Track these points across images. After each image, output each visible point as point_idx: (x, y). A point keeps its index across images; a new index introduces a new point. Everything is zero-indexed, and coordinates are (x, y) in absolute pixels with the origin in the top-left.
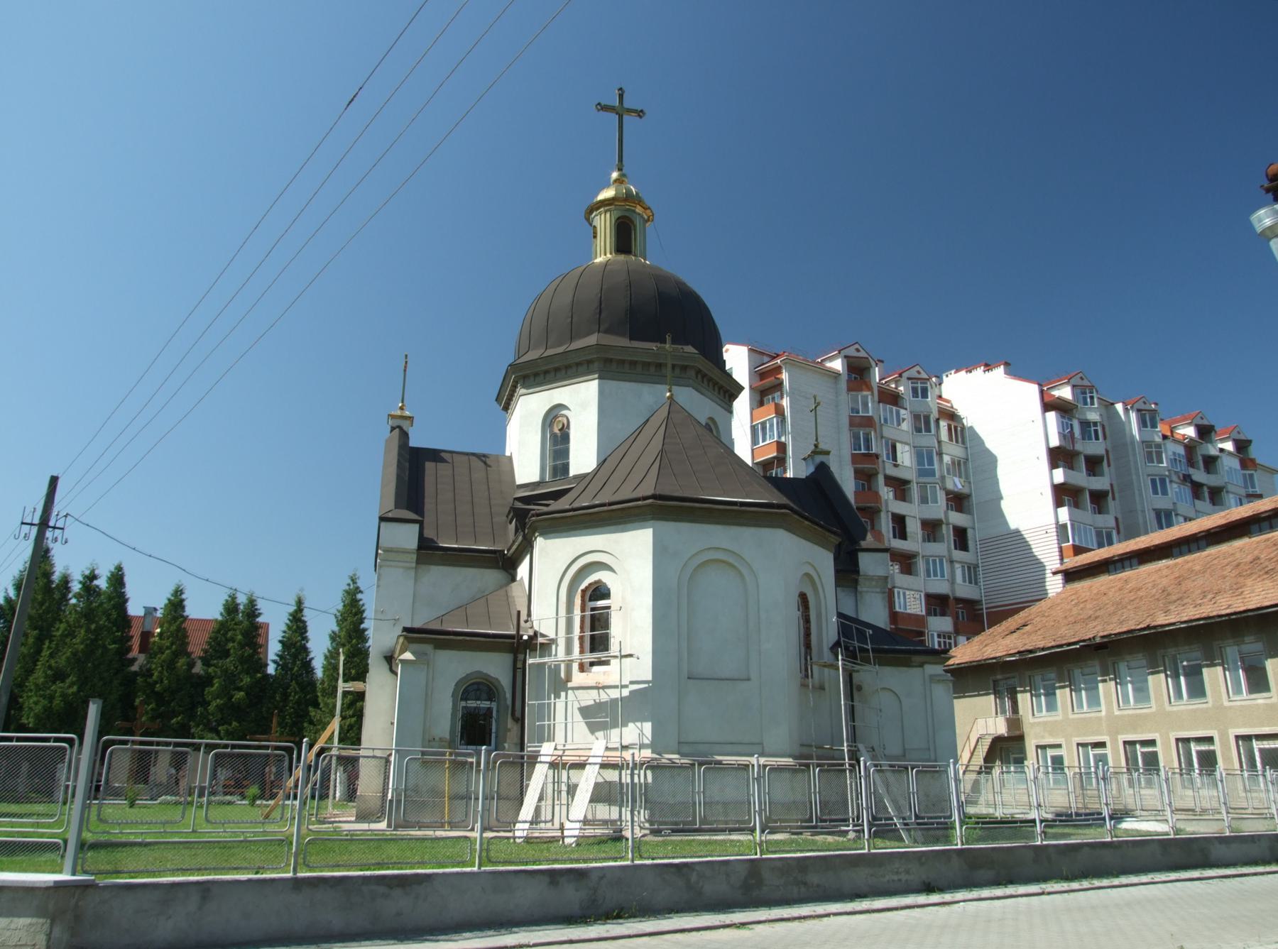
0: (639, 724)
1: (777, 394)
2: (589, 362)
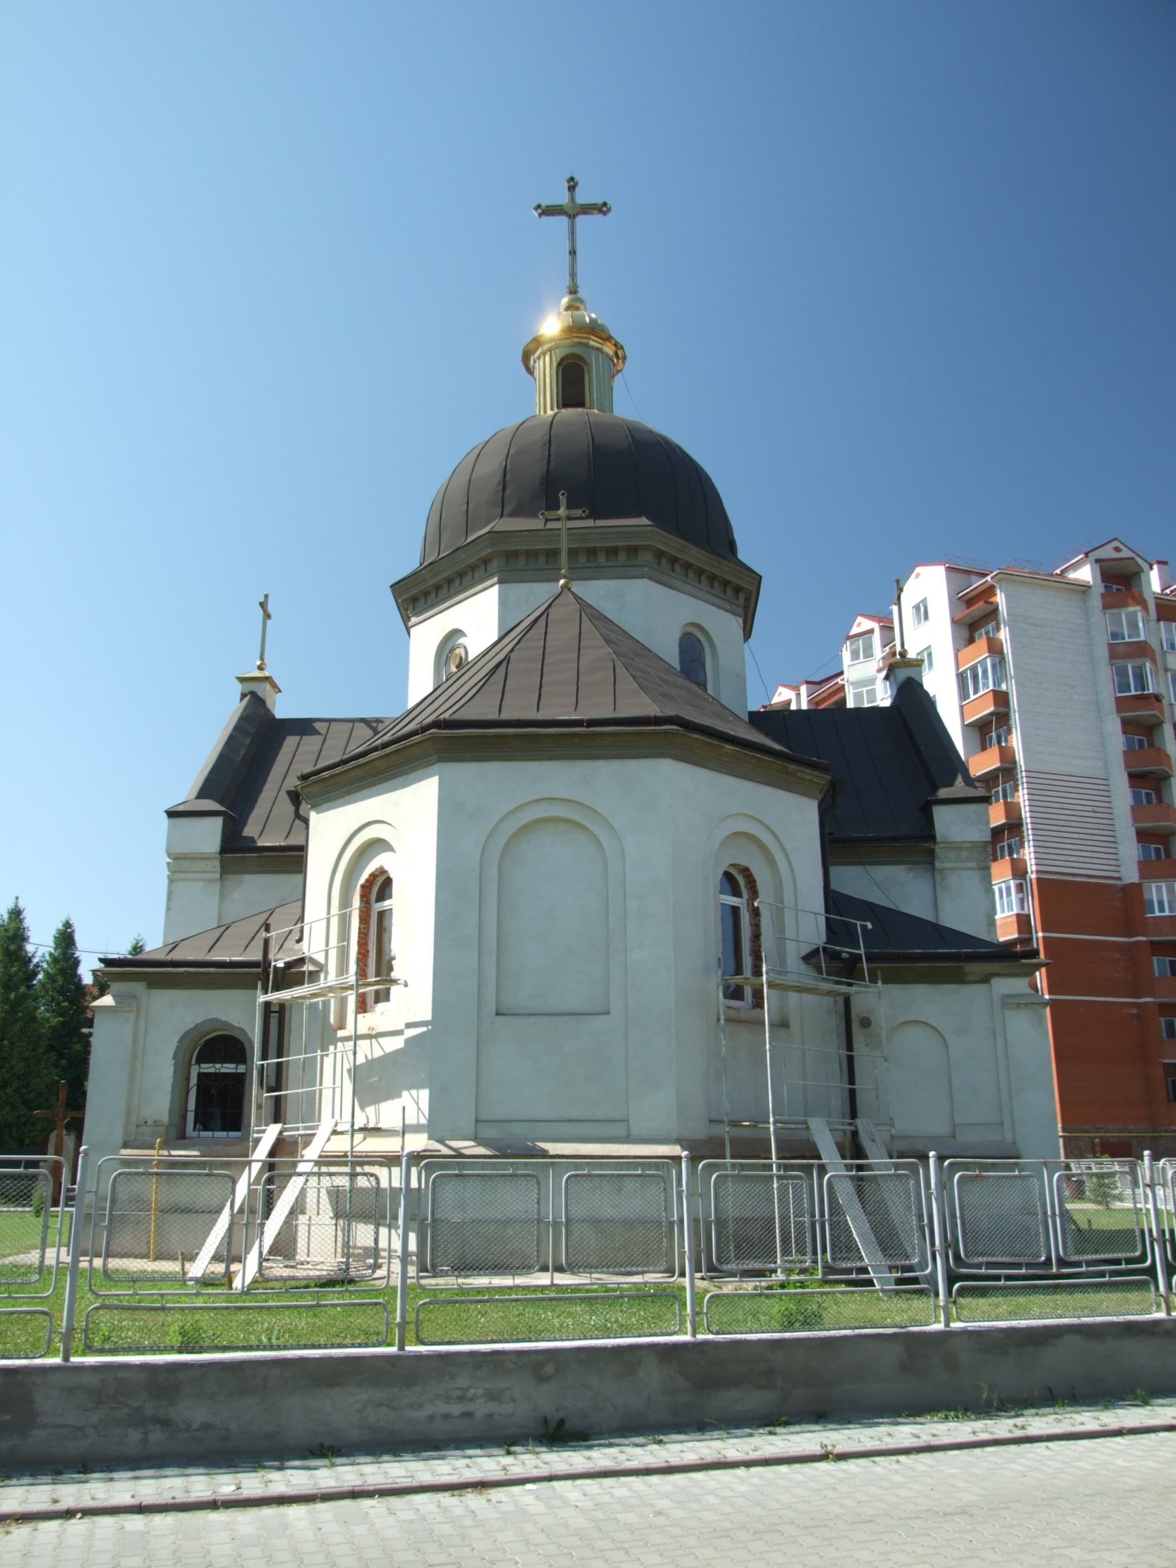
0: (414, 1092)
1: (991, 626)
2: (486, 561)
